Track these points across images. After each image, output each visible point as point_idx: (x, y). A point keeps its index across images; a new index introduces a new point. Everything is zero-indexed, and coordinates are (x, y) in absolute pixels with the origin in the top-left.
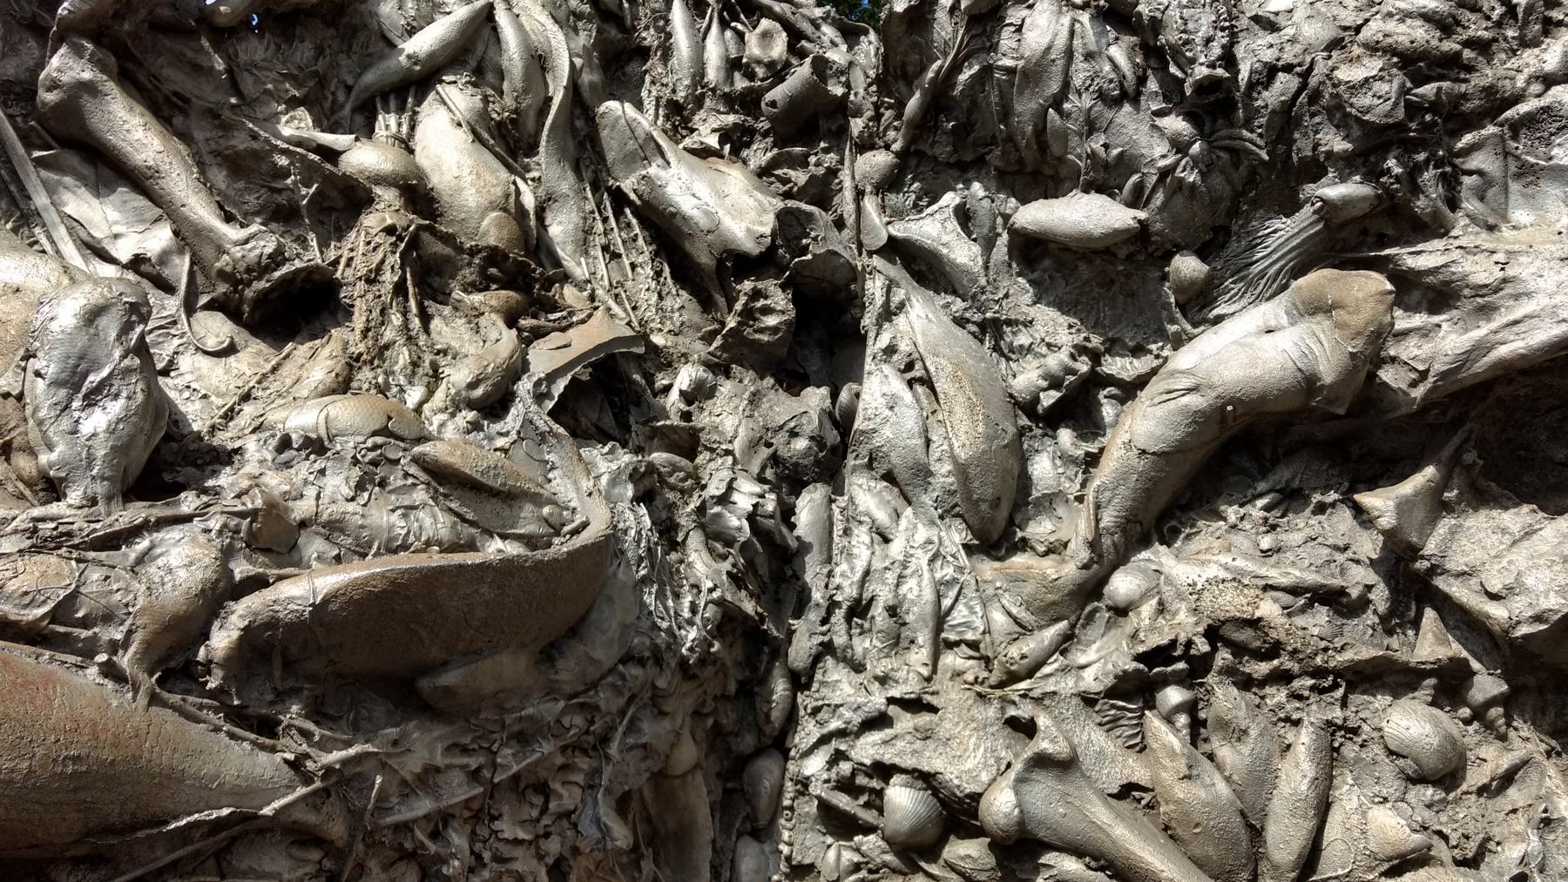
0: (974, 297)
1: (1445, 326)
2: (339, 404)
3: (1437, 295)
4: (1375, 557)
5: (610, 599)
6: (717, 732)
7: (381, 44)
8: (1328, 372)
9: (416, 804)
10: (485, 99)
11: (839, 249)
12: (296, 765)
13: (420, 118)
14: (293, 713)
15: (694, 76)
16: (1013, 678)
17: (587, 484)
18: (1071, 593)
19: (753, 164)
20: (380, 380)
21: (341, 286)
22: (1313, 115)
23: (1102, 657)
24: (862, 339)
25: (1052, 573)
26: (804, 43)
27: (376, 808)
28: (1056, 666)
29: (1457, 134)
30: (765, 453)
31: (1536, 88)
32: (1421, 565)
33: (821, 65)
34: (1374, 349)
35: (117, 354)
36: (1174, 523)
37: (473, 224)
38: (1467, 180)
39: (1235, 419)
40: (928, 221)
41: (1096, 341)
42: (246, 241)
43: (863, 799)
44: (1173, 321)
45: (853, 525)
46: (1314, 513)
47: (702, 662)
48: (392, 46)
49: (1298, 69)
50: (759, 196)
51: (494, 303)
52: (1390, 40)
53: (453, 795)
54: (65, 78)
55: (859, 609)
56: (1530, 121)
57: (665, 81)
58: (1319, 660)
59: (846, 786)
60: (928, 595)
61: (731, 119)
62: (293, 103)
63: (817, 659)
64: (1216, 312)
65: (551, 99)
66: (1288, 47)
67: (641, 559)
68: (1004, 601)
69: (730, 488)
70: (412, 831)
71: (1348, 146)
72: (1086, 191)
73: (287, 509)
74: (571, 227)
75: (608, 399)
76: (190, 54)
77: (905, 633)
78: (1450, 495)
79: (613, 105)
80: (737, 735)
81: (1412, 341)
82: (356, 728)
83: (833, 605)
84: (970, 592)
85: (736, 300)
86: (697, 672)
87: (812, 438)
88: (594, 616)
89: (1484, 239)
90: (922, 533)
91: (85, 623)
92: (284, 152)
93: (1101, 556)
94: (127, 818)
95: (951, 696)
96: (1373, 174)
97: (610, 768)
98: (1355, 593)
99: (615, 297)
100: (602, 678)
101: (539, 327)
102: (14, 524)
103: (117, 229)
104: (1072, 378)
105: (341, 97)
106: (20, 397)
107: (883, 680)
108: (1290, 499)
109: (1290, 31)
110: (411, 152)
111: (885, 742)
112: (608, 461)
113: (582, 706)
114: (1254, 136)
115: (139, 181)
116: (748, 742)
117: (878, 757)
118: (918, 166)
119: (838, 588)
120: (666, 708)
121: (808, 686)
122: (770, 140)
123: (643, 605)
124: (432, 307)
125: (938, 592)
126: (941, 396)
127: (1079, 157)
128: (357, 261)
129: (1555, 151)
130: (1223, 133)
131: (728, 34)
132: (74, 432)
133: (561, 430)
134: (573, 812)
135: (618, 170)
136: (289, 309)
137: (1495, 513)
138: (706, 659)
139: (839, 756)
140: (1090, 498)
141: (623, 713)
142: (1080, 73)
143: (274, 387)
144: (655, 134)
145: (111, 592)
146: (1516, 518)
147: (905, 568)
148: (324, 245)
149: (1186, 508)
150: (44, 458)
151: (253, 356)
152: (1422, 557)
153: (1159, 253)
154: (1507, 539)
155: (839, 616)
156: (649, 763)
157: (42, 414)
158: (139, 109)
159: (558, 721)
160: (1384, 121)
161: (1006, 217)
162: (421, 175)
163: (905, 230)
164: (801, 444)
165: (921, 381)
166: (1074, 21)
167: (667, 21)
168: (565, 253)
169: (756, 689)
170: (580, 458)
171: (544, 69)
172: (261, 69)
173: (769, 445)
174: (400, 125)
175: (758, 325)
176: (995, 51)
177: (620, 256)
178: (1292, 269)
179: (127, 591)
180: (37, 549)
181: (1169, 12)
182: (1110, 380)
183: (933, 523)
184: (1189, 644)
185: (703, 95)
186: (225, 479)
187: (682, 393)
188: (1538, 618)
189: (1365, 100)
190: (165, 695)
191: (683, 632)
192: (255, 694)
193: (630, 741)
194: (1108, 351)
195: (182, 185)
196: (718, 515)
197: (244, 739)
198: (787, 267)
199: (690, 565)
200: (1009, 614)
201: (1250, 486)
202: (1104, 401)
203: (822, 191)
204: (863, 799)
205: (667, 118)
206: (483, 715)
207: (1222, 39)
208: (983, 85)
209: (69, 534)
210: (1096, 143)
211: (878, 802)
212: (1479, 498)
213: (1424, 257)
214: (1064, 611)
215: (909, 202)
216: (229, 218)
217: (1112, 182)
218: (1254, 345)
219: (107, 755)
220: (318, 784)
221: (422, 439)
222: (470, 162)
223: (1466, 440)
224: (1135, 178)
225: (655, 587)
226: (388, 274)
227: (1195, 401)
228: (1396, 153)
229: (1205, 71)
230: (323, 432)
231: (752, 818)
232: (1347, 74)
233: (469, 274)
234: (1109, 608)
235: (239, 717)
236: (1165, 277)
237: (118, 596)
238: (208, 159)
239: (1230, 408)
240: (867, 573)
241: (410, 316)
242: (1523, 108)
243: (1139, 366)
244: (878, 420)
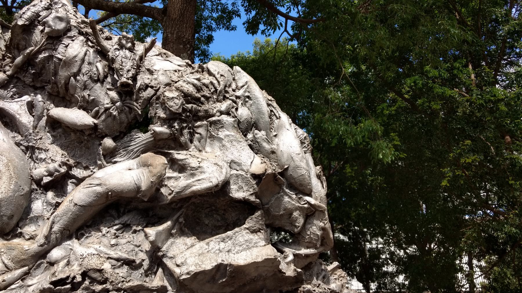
0: (26, 136)
1: (182, 177)
3: (181, 167)
4: (148, 250)
8: (144, 187)
18: (31, 256)
22: (157, 104)
25: (26, 247)
28: (17, 285)
29: (196, 121)
31: (218, 114)
32: (160, 254)
34: (160, 182)
36: (83, 232)
39: (111, 197)
40: (15, 103)
41: (71, 162)
44: (100, 160)
46: (132, 233)
49: (155, 88)
52: (182, 88)
56: (214, 123)
58: (119, 285)
64: (115, 160)
66: (153, 81)
68: (3, 258)
71: (164, 116)
72: (79, 109)
78: (173, 231)
81: (172, 181)
89: (197, 154)
93: (49, 242)
96: (171, 127)
98: (138, 262)
104: (57, 173)
108: (126, 227)
109: (155, 76)
114: (138, 105)
118: (16, 83)
127: (79, 96)
129: (220, 133)
130: (128, 101)
137: (185, 238)
140: (51, 219)
142: (85, 68)
146: (190, 240)
149: (88, 227)
152: (161, 251)
153: (100, 136)
154: (186, 247)
160: (176, 111)
161: (48, 110)
163: (3, 105)
166: (87, 50)
176: (56, 51)
178: (142, 151)
181: (118, 58)
182: (74, 177)
184: (74, 277)
188: (188, 273)
189: (171, 104)
194: (76, 166)
200: (4, 263)
201: (113, 221)
202: (69, 184)
207: (133, 72)
208: (49, 61)
210: (86, 93)
212: (182, 233)
213: (179, 155)
214: (28, 263)
217: (89, 108)
218: (124, 173)
223: (181, 214)
224: (97, 108)
227: (99, 189)
228: (178, 122)
229: (125, 80)
232: (167, 94)
234: (48, 262)
236: (100, 144)
239: (110, 193)
242: (214, 119)
243: (85, 173)
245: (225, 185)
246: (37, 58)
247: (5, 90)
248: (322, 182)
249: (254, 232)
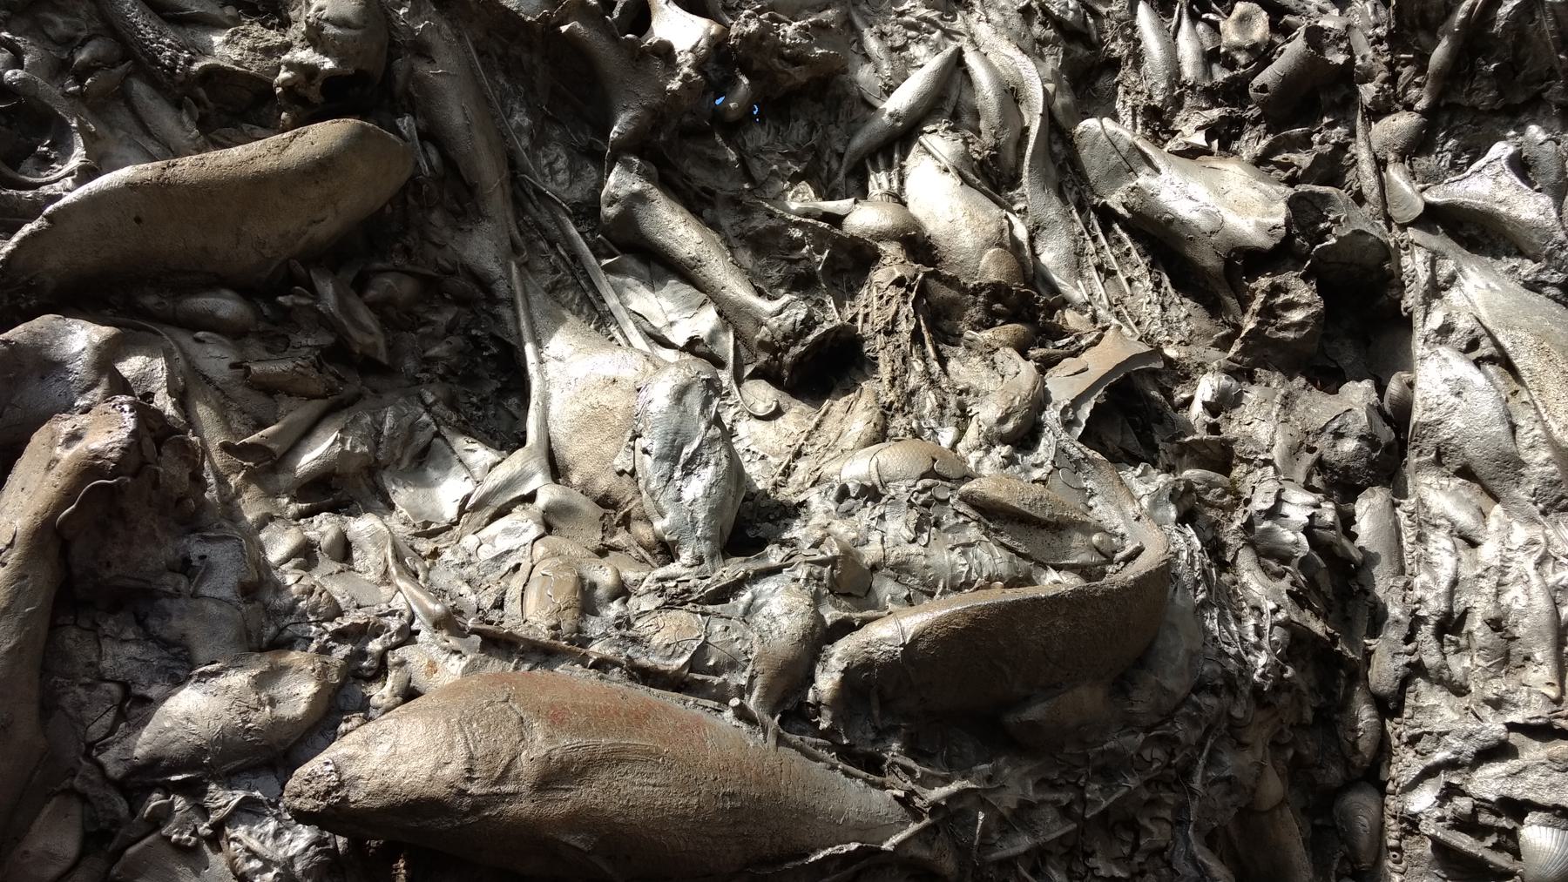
0: (1550, 256)
2: (887, 452)
5: (1173, 626)
7: (863, 109)
9: (1015, 841)
10: (966, 142)
11: (1366, 227)
12: (906, 801)
13: (907, 171)
14: (894, 750)
15: (1169, 78)
17: (1132, 509)
19: (1246, 155)
20: (914, 425)
21: (863, 341)
24: (1406, 324)
26: (1287, 18)
27: (981, 844)
30: (1308, 459)
33: (1316, 36)
35: (703, 426)
37: (972, 264)
40: (1475, 178)
42: (781, 312)
43: (1491, 840)
45: (1427, 530)
47: (1276, 688)
48: (873, 108)
50: (1263, 186)
51: (1002, 337)
53: (1049, 832)
54: (621, 193)
55: (1451, 625)
57: (1139, 88)
59: (1466, 824)
60: (1541, 603)
61: (1215, 113)
62: (795, 179)
63: (1405, 682)
65: (1027, 129)
67: (1197, 583)
69: (1279, 500)
70: (1016, 868)
73: (859, 554)
74: (1062, 252)
75: (1132, 416)
76: (709, 152)
77: (1516, 649)
79: (1091, 123)
80: (1320, 767)
82: (950, 765)
85: (1252, 297)
86: (1272, 699)
87: (1361, 438)
88: (1159, 645)
90: (1520, 534)
91: (716, 671)
92: (797, 225)
94: (776, 851)
97: (1196, 802)
99: (1122, 315)
100: (1177, 708)
101: (1049, 355)
102: (645, 583)
103: (671, 318)
105: (835, 165)
106: (633, 473)
107: (1498, 704)
110: (905, 204)
111: (1512, 775)
112: (1146, 484)
113: (1160, 738)
116: (1335, 774)
117: (1505, 793)
118: (1450, 121)
119: (1420, 601)
120: (1245, 739)
121: (1398, 712)
122: (1262, 127)
123: (1206, 631)
124: (947, 350)
125: (1554, 599)
126: (1526, 376)
128: (874, 315)
131: (1201, 27)
132: (679, 499)
133: (1098, 456)
134: (1166, 849)
135: (1101, 188)
136: (822, 370)
138: (1280, 685)
139: (1449, 792)
141: (1201, 745)
143: (821, 442)
144: (1139, 143)
145: (732, 641)
147: (1505, 574)
148: (840, 306)
150: (659, 525)
151: (797, 417)
155: (1426, 633)
156: (1234, 797)
157: (653, 486)
158: (678, 208)
159: (1139, 755)
162: (917, 225)
164: (1349, 445)
165: (1491, 359)
167: (1134, 28)
169: (1336, 717)
170: (1122, 483)
171: (1017, 101)
172: (765, 153)
173: (1311, 450)
174: (890, 181)
175: (1280, 322)
177: (1114, 273)
179: (745, 640)
180: (669, 606)
183: (1532, 520)
185: (1181, 95)
186: (797, 531)
187: (1205, 405)
190: (788, 736)
191: (1252, 658)
192: (859, 734)
193: (1212, 774)
195: (720, 269)
196: (1268, 531)
197: (857, 777)
198: (1307, 256)
199: (1244, 586)
203: (1333, 168)
204: (1491, 840)
205: (1146, 125)
206: (1067, 750)
208: (1532, 14)
209: (688, 591)
211: (1510, 843)
215: (1445, 163)
216: (760, 293)
219: (754, 791)
220: (927, 820)
221: (967, 477)
222: (962, 204)
225: (1216, 611)
226: (904, 323)
230: (876, 480)
233: (975, 313)
235: (847, 754)
237: (738, 645)
238: (735, 243)
240: (1455, 583)
241: (929, 361)
244: (1442, 409)
246: (1492, 22)
247: (1429, 155)
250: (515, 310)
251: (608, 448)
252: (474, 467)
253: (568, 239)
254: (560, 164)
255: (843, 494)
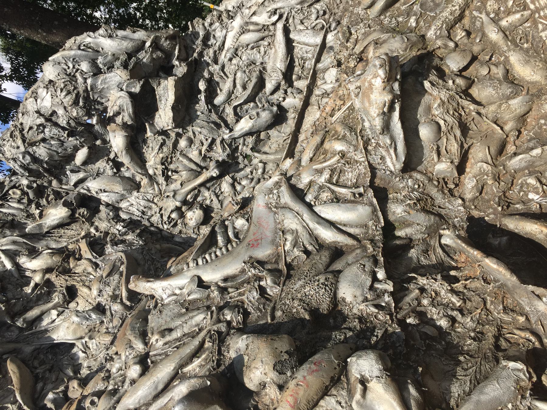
6: (157, 240)
16: (161, 193)
23: (161, 180)
30: (111, 220)
31: (86, 84)
38: (99, 99)
55: (143, 213)
60: (144, 201)
63: (149, 222)
69: (118, 230)
81: (124, 118)
83: (141, 217)
84: (145, 195)
90: (133, 198)
95: (160, 204)
96: (94, 115)
107: (156, 213)
115: (43, 314)
128: (62, 282)
131: (10, 200)
136: (71, 293)
138: (145, 241)
139: (165, 223)
146: (157, 116)
149: (141, 157)
150: (98, 322)
151: (79, 300)
155: (143, 216)
162: (42, 270)
164: (111, 213)
168: (60, 246)
171: (16, 242)
182: (114, 158)
212: (153, 117)
218: (117, 141)
221: (102, 276)
227: (124, 152)
231: (170, 237)
233: (66, 265)
235: (138, 303)
245: (131, 95)
248: (138, 31)
249: (159, 84)
250: (43, 344)
251: (81, 329)
252: (78, 351)
253: (28, 334)
254: (10, 334)
255: (99, 295)
